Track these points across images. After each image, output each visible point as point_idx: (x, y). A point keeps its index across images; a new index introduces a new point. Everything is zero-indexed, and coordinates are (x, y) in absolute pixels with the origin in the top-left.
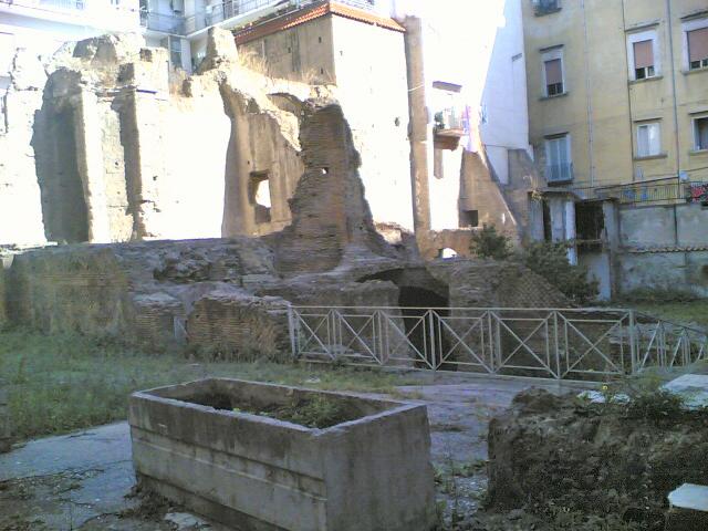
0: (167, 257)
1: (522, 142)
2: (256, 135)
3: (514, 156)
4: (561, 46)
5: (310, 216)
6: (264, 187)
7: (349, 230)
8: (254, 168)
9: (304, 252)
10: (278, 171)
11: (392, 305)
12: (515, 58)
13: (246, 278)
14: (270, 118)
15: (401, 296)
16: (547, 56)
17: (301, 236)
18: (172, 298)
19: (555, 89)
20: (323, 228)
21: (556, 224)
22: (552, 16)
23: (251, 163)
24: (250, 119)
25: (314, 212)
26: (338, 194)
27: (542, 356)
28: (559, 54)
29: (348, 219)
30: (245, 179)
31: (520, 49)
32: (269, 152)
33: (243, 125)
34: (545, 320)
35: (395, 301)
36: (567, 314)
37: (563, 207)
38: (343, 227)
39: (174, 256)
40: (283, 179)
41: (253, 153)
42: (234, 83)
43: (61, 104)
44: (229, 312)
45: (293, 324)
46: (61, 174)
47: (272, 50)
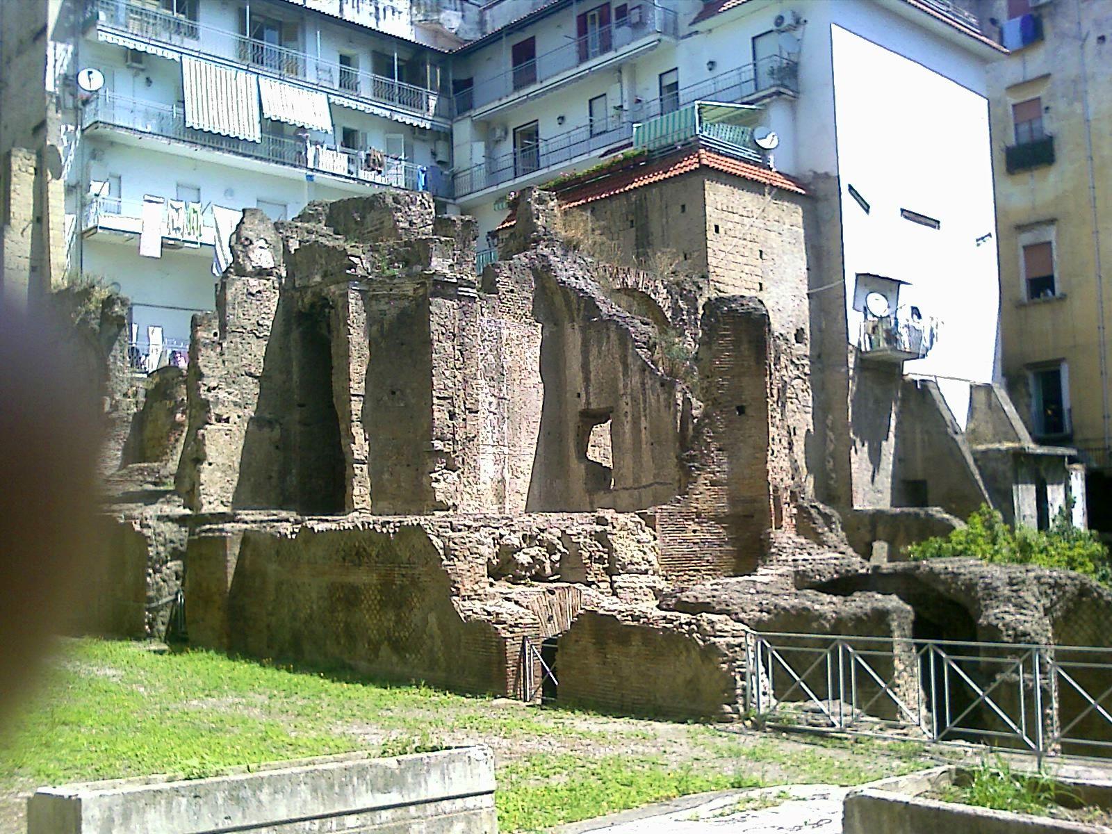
0: (504, 541)
2: (594, 351)
4: (1052, 221)
6: (601, 435)
8: (588, 403)
10: (627, 409)
13: (619, 580)
14: (619, 326)
16: (1027, 238)
19: (1041, 286)
23: (583, 395)
24: (583, 330)
28: (1051, 234)
30: (572, 422)
32: (616, 379)
33: (574, 338)
35: (908, 632)
36: (951, 650)
39: (515, 540)
40: (636, 423)
41: (587, 380)
42: (568, 271)
43: (308, 299)
46: (301, 406)
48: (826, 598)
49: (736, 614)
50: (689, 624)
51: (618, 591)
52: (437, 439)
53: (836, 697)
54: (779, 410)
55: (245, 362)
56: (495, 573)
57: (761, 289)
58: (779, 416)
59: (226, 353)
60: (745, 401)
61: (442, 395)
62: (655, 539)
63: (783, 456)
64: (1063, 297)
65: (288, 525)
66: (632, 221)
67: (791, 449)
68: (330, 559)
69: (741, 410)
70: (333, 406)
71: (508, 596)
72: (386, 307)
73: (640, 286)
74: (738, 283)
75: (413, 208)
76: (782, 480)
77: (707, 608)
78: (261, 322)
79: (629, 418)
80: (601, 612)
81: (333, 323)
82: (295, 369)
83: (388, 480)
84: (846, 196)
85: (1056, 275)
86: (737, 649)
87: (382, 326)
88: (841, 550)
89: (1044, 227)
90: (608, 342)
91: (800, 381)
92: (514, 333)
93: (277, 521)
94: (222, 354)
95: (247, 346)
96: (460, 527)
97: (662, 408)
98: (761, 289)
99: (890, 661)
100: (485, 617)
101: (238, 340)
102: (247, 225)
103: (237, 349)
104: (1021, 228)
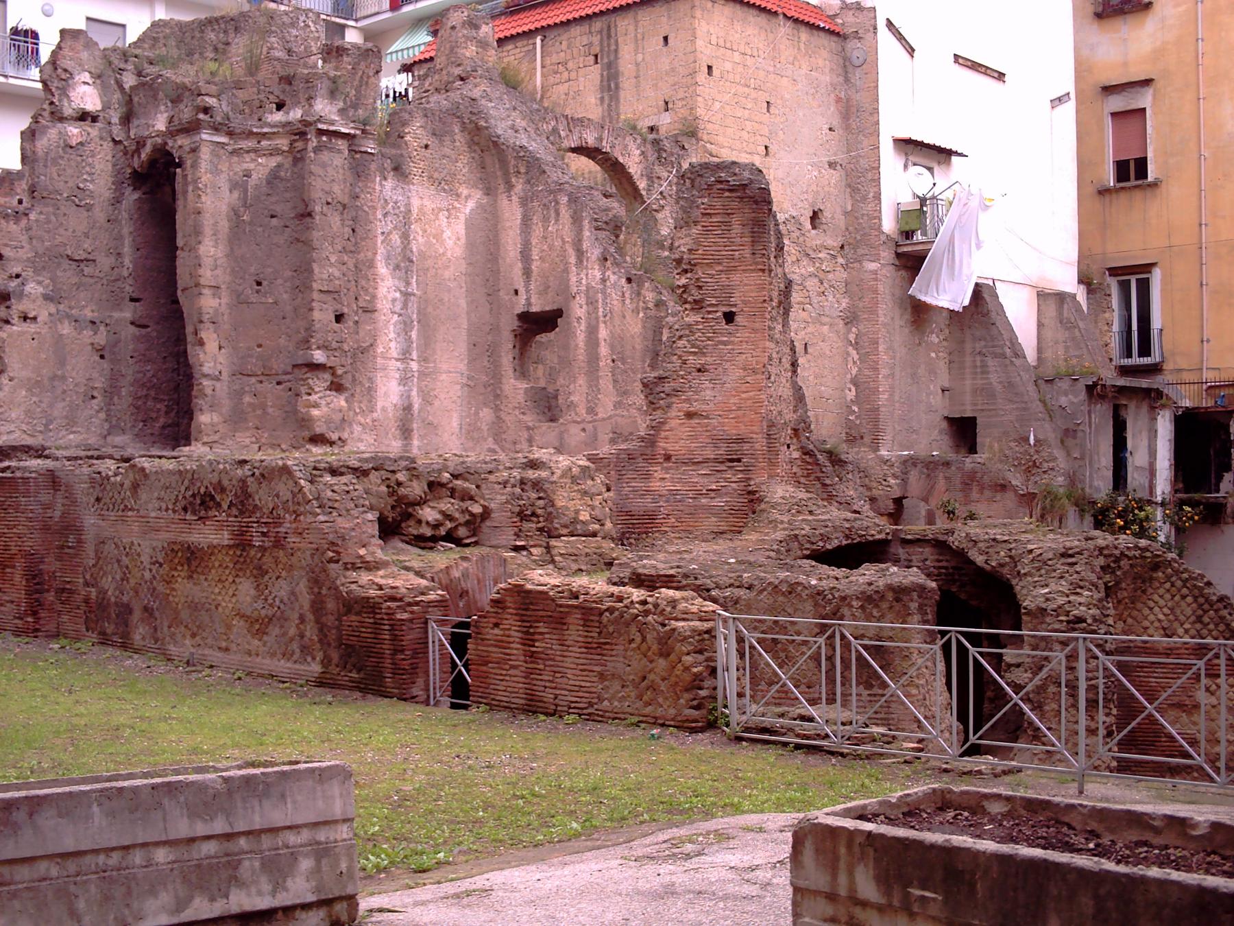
1: (1066, 280)
2: (537, 231)
3: (1051, 310)
4: (1147, 82)
5: (690, 415)
7: (772, 449)
8: (529, 304)
9: (673, 493)
11: (925, 622)
12: (1059, 101)
13: (560, 545)
15: (940, 604)
16: (1118, 103)
17: (668, 458)
18: (424, 582)
20: (715, 441)
21: (1137, 459)
22: (1130, 19)
23: (522, 291)
24: (524, 202)
25: (696, 407)
26: (754, 371)
27: (1193, 742)
28: (1145, 100)
29: (771, 425)
31: (1067, 84)
32: (566, 271)
34: (1201, 664)
36: (976, 640)
37: (1154, 420)
38: (760, 443)
39: (416, 489)
40: (592, 331)
41: (527, 273)
44: (575, 619)
45: (726, 650)
46: (133, 300)
47: (555, 59)
48: (825, 569)
49: (708, 590)
50: (644, 603)
51: (557, 558)
52: (319, 348)
53: (831, 700)
54: (780, 321)
55: (59, 239)
56: (388, 529)
57: (767, 154)
58: (779, 327)
59: (35, 228)
60: (735, 305)
61: (325, 288)
62: (609, 490)
63: (784, 381)
64: (1155, 185)
65: (109, 462)
66: (596, 56)
67: (794, 372)
68: (167, 510)
69: (729, 317)
70: (177, 302)
71: (407, 564)
72: (252, 166)
73: (604, 143)
74: (738, 145)
75: (294, 32)
76: (780, 413)
77: (668, 581)
78: (81, 185)
79: (583, 327)
80: (529, 586)
81: (178, 187)
82: (127, 249)
83: (250, 404)
84: (883, 33)
85: (1150, 155)
86: (706, 636)
87: (246, 191)
88: (855, 508)
89: (1139, 89)
90: (557, 220)
91: (816, 280)
92: (429, 205)
93: (98, 458)
94: (29, 229)
95: (62, 219)
96: (343, 470)
97: (628, 314)
98: (767, 154)
99: (1159, 731)
100: (373, 593)
101: (51, 209)
102: (66, 52)
103: (49, 222)
104: (1109, 90)
